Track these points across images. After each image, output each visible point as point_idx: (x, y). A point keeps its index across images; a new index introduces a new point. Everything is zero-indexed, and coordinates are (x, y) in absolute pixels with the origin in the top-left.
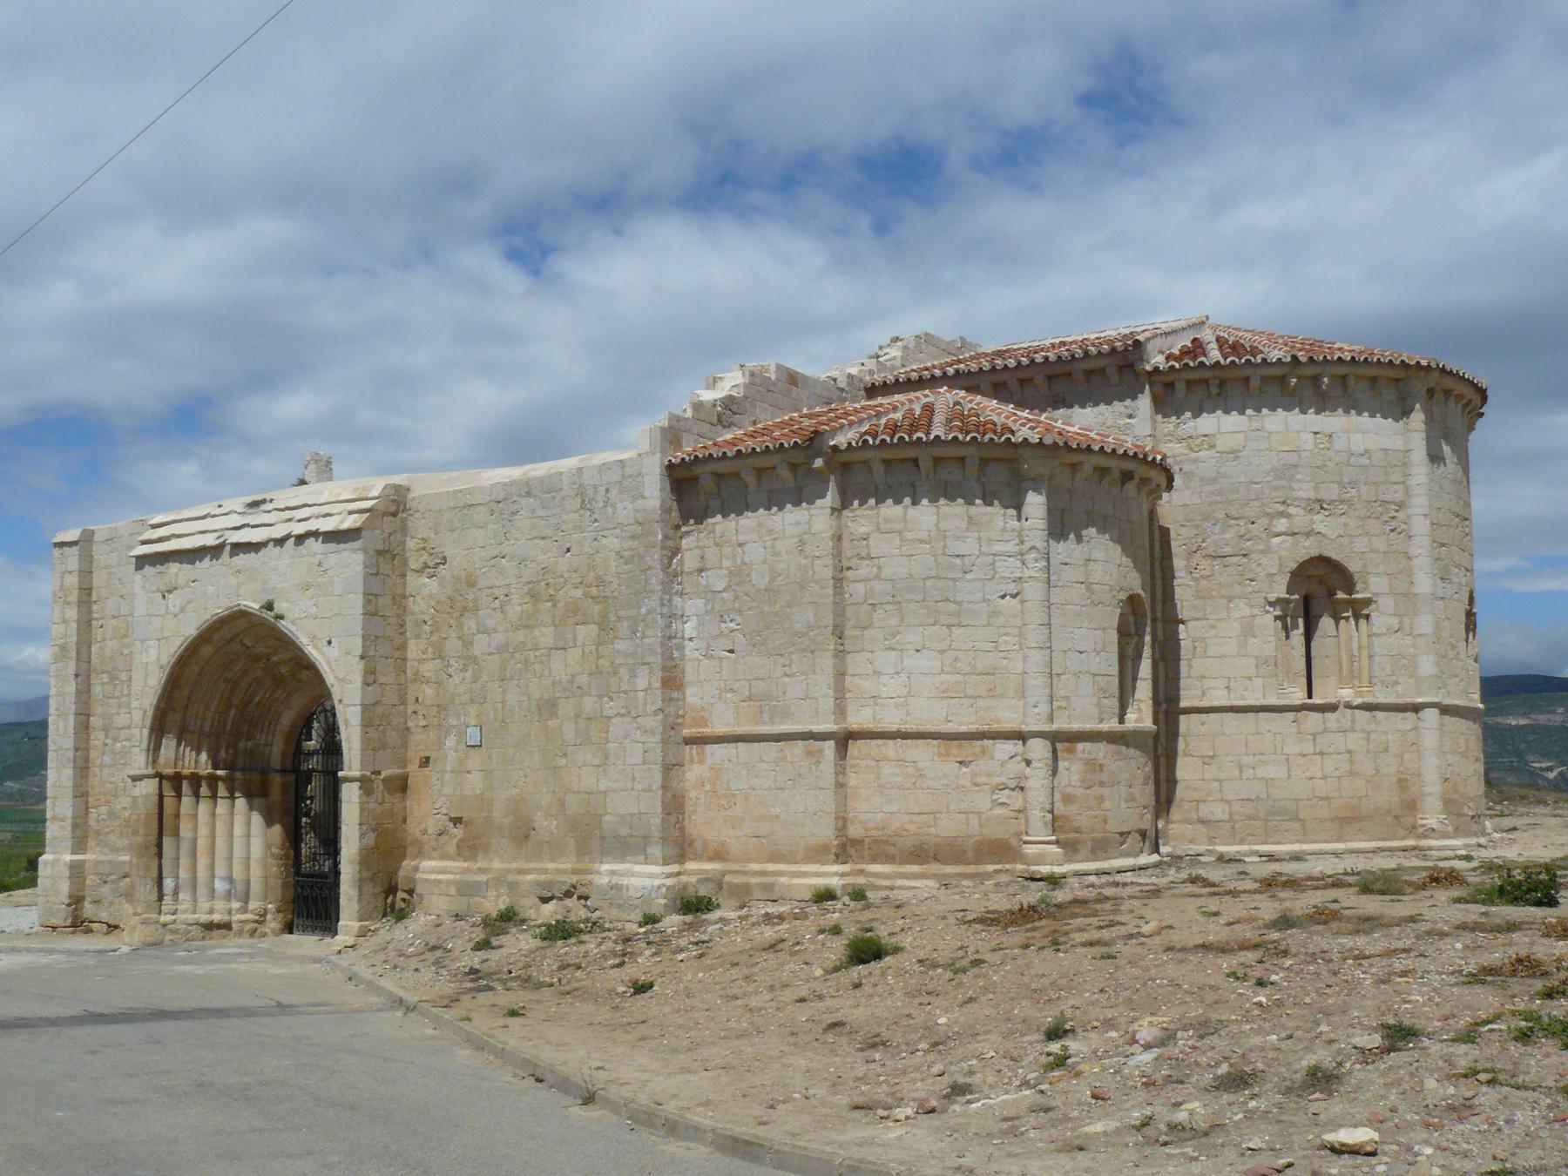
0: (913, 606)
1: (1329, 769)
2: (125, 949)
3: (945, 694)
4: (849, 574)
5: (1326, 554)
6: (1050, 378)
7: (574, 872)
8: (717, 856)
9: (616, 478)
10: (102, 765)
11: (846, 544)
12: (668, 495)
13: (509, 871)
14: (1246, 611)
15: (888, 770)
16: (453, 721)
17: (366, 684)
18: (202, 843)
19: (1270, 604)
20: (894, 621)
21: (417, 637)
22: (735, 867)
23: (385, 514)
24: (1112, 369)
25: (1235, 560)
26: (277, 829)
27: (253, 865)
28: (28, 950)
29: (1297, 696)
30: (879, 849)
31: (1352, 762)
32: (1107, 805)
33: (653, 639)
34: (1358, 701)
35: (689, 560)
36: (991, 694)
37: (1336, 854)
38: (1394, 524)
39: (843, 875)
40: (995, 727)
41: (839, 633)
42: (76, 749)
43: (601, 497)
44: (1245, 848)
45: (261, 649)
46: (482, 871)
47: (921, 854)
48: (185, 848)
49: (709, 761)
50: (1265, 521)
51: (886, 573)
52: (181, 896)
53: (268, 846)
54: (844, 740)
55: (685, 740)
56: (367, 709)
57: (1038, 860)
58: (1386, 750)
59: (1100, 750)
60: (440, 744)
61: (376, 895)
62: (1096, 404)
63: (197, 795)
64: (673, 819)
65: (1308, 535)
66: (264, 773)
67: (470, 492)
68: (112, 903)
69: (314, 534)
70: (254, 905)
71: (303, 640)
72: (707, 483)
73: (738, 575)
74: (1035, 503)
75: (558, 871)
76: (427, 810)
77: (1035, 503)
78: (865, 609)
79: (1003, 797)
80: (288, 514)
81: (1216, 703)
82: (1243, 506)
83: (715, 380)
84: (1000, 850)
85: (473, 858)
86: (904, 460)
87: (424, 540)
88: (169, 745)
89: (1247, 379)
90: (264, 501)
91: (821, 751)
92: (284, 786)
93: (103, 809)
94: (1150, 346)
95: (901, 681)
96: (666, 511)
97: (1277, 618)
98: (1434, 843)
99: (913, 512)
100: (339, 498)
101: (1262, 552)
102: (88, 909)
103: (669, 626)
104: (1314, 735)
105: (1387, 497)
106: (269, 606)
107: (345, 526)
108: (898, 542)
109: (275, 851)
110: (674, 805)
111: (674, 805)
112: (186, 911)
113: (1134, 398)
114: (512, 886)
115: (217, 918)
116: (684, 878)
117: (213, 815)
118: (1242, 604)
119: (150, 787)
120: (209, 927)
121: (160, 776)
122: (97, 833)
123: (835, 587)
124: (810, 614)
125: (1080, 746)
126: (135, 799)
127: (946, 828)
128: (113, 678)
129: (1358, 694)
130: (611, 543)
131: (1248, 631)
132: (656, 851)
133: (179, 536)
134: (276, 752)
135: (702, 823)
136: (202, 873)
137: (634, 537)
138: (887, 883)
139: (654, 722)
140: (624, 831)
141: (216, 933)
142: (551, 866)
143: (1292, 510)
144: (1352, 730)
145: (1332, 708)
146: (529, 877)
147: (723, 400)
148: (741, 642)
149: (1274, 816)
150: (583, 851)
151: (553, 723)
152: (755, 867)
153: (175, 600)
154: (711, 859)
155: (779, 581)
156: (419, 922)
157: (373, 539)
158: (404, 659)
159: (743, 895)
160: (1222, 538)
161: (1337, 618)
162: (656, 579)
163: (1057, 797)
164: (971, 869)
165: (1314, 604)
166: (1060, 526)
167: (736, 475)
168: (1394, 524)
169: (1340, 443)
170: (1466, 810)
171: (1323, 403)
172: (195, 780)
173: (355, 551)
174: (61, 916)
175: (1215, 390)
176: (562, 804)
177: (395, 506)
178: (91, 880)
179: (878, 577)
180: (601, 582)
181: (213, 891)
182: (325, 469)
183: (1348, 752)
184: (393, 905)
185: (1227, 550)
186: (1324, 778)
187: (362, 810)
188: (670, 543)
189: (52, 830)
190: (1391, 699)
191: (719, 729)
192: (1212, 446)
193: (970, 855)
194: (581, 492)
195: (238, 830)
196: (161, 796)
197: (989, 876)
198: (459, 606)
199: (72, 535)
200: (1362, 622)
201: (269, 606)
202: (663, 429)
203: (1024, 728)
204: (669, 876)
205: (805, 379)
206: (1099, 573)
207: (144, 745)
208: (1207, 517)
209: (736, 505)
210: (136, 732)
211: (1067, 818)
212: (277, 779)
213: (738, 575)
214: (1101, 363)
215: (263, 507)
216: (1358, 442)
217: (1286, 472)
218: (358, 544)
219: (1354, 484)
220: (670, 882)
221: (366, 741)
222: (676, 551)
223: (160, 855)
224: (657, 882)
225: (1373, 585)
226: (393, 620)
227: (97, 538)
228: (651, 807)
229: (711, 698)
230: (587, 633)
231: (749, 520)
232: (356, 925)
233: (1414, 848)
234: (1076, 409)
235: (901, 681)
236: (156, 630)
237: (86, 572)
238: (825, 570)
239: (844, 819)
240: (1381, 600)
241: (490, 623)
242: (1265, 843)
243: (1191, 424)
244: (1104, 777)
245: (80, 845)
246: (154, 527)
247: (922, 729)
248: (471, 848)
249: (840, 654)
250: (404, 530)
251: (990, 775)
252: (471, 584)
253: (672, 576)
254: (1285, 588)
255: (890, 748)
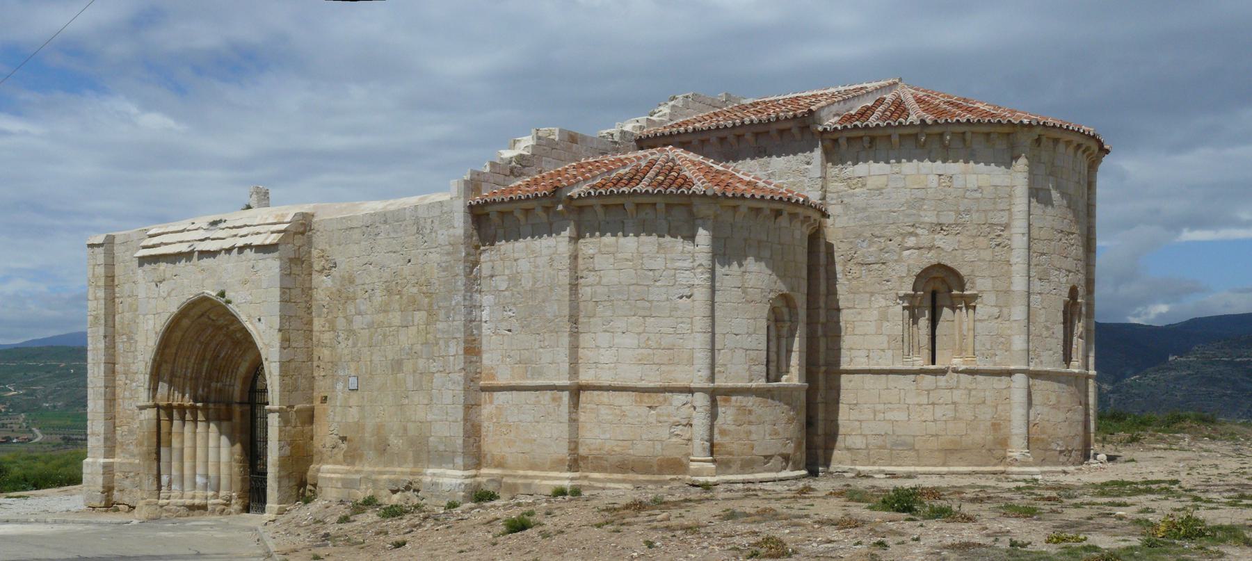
0: (621, 303)
1: (938, 415)
2: (135, 522)
3: (640, 361)
4: (581, 281)
5: (943, 262)
6: (757, 135)
7: (412, 474)
8: (500, 465)
9: (438, 213)
10: (124, 398)
11: (580, 261)
12: (470, 226)
13: (373, 472)
14: (883, 303)
15: (603, 411)
16: (341, 373)
17: (283, 348)
18: (187, 452)
19: (900, 298)
20: (609, 313)
21: (319, 316)
22: (509, 472)
23: (295, 233)
24: (790, 131)
25: (876, 266)
26: (238, 447)
27: (222, 467)
28: (73, 522)
29: (921, 361)
30: (599, 463)
31: (956, 411)
32: (754, 437)
33: (459, 321)
34: (963, 367)
35: (485, 268)
36: (671, 362)
37: (940, 475)
38: (999, 240)
39: (572, 479)
40: (673, 384)
41: (574, 319)
42: (106, 387)
43: (428, 226)
44: (876, 468)
45: (221, 322)
46: (357, 472)
47: (623, 466)
48: (175, 454)
49: (496, 403)
50: (899, 239)
51: (604, 281)
52: (173, 487)
53: (232, 454)
54: (576, 391)
55: (477, 389)
56: (282, 364)
57: (698, 473)
58: (984, 402)
59: (750, 401)
60: (333, 388)
61: (291, 488)
62: (787, 155)
63: (183, 419)
64: (472, 440)
65: (930, 249)
66: (229, 404)
67: (350, 219)
68: (131, 492)
69: (249, 246)
70: (222, 493)
71: (243, 318)
72: (494, 217)
73: (514, 279)
74: (703, 236)
75: (403, 473)
76: (325, 433)
77: (703, 236)
78: (591, 304)
79: (678, 430)
80: (235, 231)
81: (859, 367)
82: (883, 228)
83: (515, 142)
84: (676, 466)
85: (353, 464)
86: (617, 205)
87: (323, 251)
88: (163, 388)
89: (889, 136)
90: (220, 221)
91: (561, 398)
92: (242, 414)
93: (125, 428)
94: (823, 114)
95: (612, 354)
96: (468, 236)
97: (904, 308)
98: (1015, 469)
99: (622, 240)
100: (265, 223)
101: (896, 261)
102: (116, 495)
103: (470, 313)
104: (929, 391)
105: (995, 221)
106: (222, 294)
107: (267, 242)
108: (612, 260)
109: (237, 457)
110: (473, 432)
111: (473, 432)
112: (177, 497)
113: (812, 151)
114: (375, 482)
115: (197, 502)
116: (479, 479)
117: (195, 433)
118: (880, 298)
119: (151, 413)
120: (192, 508)
121: (158, 407)
122: (122, 444)
123: (571, 289)
124: (556, 307)
125: (734, 398)
126: (141, 422)
127: (640, 450)
128: (130, 338)
129: (965, 362)
130: (435, 257)
131: (883, 317)
132: (459, 461)
133: (166, 244)
134: (237, 391)
135: (492, 444)
136: (187, 472)
137: (448, 254)
138: (601, 485)
139: (459, 377)
140: (442, 448)
141: (197, 512)
142: (399, 469)
143: (919, 231)
144: (957, 388)
145: (943, 372)
146: (385, 477)
147: (516, 157)
148: (515, 324)
149: (899, 447)
150: (417, 460)
151: (400, 375)
152: (521, 472)
153: (164, 287)
154: (496, 467)
155: (538, 285)
156: (316, 506)
157: (288, 250)
158: (311, 331)
159: (513, 490)
160: (868, 251)
161: (953, 309)
162: (461, 281)
163: (716, 431)
164: (656, 478)
165: (939, 297)
166: (723, 253)
167: (512, 212)
168: (999, 240)
169: (958, 182)
170: (1054, 446)
171: (946, 155)
172: (182, 409)
173: (274, 259)
174: (98, 500)
175: (867, 145)
176: (405, 430)
177: (303, 228)
178: (118, 476)
179: (599, 283)
180: (429, 283)
181: (195, 483)
182: (264, 198)
183: (953, 403)
184: (303, 494)
185: (871, 259)
186: (935, 421)
187: (280, 431)
188: (472, 258)
189: (91, 441)
190: (989, 366)
191: (501, 381)
192: (864, 185)
193: (655, 468)
194: (417, 221)
195: (212, 443)
196: (159, 420)
197: (667, 482)
198: (343, 296)
199: (99, 239)
200: (971, 311)
201: (222, 294)
202: (466, 182)
203: (692, 385)
204: (467, 477)
205: (584, 138)
206: (751, 280)
207: (146, 386)
208: (858, 236)
209: (514, 234)
210: (141, 377)
211: (722, 445)
212: (237, 409)
213: (514, 279)
214: (787, 125)
215: (222, 225)
216: (972, 182)
217: (916, 203)
218: (276, 254)
219: (968, 211)
220: (468, 481)
221: (283, 386)
222: (476, 263)
223: (158, 459)
224: (459, 481)
225: (980, 284)
226: (304, 305)
227: (117, 241)
228: (457, 431)
229: (497, 362)
230: (420, 316)
231: (521, 244)
232: (276, 506)
233: (1003, 473)
234: (774, 157)
235: (612, 354)
236: (153, 307)
237: (110, 265)
238: (564, 278)
239: (576, 443)
240: (985, 296)
241: (363, 308)
242: (890, 465)
243: (851, 169)
244: (752, 418)
245: (110, 451)
246: (151, 236)
247: (624, 384)
248: (352, 457)
249: (575, 334)
250: (310, 243)
251: (669, 416)
252: (352, 282)
253: (473, 280)
254: (911, 287)
255: (605, 396)
